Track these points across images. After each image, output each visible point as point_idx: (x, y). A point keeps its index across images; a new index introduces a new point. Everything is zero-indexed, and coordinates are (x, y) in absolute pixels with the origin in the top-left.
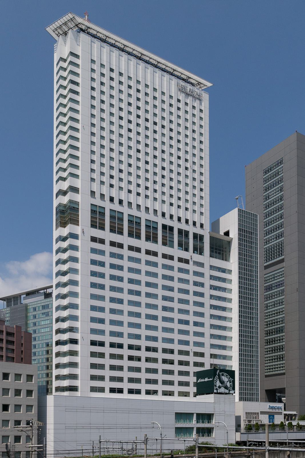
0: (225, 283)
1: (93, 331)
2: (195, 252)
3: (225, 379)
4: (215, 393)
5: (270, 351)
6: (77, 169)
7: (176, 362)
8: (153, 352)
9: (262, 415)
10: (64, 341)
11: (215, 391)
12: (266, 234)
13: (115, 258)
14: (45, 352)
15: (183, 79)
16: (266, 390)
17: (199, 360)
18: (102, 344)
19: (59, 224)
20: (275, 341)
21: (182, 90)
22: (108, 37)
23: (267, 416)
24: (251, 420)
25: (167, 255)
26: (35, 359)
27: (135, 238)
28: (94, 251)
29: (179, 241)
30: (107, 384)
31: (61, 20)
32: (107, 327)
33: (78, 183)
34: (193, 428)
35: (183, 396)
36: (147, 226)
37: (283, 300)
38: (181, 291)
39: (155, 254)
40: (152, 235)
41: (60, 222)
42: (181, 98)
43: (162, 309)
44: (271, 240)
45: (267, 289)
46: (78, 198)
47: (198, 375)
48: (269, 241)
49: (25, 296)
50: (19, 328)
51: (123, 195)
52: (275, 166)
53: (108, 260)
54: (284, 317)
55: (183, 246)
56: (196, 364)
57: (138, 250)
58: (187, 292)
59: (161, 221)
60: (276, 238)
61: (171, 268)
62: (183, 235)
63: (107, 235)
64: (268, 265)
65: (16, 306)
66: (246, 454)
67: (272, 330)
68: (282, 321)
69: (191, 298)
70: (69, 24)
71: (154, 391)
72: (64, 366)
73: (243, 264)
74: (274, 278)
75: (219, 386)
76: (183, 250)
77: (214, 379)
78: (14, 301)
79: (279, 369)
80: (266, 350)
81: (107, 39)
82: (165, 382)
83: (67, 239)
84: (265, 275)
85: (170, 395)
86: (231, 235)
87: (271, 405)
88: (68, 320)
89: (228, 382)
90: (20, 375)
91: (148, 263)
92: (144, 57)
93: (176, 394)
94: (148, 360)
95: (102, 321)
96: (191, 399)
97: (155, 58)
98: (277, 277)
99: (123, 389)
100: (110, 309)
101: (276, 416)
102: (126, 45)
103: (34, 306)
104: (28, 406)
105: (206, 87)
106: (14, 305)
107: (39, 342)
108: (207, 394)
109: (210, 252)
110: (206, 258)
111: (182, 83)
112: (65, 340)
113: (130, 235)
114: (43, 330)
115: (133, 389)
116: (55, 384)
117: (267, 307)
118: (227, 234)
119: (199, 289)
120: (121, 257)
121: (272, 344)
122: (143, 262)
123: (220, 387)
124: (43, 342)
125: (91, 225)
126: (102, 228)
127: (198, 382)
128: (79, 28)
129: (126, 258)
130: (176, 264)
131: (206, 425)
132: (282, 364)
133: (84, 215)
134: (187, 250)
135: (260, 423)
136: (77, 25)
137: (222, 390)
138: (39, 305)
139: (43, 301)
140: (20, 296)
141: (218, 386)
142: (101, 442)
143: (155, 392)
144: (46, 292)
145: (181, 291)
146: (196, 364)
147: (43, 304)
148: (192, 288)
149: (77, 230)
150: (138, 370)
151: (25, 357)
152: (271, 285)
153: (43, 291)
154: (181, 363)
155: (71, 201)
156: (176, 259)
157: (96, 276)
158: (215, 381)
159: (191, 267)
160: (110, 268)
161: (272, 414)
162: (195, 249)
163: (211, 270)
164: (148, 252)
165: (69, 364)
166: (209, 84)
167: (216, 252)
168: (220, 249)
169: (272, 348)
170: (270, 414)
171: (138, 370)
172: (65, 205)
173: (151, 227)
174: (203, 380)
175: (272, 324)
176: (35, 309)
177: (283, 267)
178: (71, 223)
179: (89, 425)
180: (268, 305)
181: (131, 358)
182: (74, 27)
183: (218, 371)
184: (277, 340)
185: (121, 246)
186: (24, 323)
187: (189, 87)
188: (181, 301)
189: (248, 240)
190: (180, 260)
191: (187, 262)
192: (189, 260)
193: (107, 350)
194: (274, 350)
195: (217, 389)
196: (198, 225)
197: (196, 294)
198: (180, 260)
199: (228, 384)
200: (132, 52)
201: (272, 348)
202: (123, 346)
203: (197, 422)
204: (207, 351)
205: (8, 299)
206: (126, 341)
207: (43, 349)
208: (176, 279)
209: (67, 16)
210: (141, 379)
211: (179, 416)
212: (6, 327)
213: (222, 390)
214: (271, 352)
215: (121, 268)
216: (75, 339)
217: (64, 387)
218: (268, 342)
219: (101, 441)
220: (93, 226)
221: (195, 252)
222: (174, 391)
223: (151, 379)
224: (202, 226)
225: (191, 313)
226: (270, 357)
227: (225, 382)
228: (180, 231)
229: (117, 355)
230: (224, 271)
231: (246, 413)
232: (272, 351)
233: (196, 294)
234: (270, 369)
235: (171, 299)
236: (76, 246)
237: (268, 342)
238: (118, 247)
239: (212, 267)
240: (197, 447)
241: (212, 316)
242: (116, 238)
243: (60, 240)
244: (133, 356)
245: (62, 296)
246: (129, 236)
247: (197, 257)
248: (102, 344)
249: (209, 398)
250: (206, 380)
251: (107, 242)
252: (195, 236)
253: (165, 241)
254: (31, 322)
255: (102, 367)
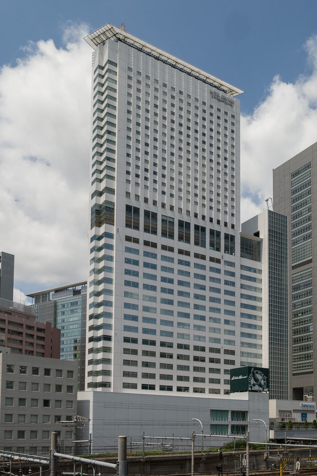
0: (256, 282)
1: (127, 328)
2: (226, 252)
3: (259, 377)
4: (249, 391)
5: (297, 350)
6: (113, 171)
7: (207, 360)
8: (184, 349)
9: (296, 414)
10: (98, 337)
11: (250, 389)
12: (294, 235)
13: (149, 257)
14: (73, 348)
15: (215, 87)
16: (293, 388)
17: (229, 357)
18: (135, 341)
19: (95, 223)
20: (302, 340)
21: (214, 96)
22: (144, 46)
23: (300, 414)
24: (284, 419)
25: (199, 254)
26: (63, 355)
27: (169, 238)
28: (128, 250)
29: (225, 245)
30: (140, 381)
31: (100, 30)
32: (140, 325)
33: (114, 185)
34: (228, 425)
35: (214, 393)
36: (163, 220)
37: (311, 300)
38: (212, 289)
39: (188, 253)
40: (184, 235)
41: (96, 221)
42: (213, 105)
43: (194, 307)
44: (299, 241)
45: (294, 289)
46: (114, 199)
47: (233, 372)
48: (297, 242)
49: (53, 292)
50: (48, 324)
51: (158, 197)
52: (303, 169)
53: (142, 259)
54: (312, 316)
55: (215, 246)
56: (227, 362)
57: (171, 249)
58: (218, 291)
59: (177, 217)
60: (304, 239)
61: (203, 267)
62: (214, 236)
63: (141, 235)
64: (296, 265)
65: (44, 303)
66: (284, 452)
67: (300, 329)
68: (310, 320)
69: (222, 297)
70: (107, 33)
71: (185, 387)
72: (97, 362)
73: (280, 266)
74: (302, 278)
75: (254, 384)
76: (214, 250)
77: (248, 377)
78: (43, 297)
79: (302, 368)
80: (294, 349)
81: (177, 65)
82: (196, 380)
83: (103, 238)
84: (292, 275)
85: (201, 392)
86: (261, 236)
87: (304, 404)
88: (102, 317)
89: (263, 380)
90: (61, 371)
91: (180, 262)
92: (179, 66)
93: (207, 391)
94: (179, 357)
95: (135, 318)
96: (222, 396)
97: (189, 66)
98: (304, 277)
99: (172, 386)
100: (143, 307)
101: (308, 415)
102: (161, 54)
103: (63, 303)
104: (21, 400)
105: (237, 94)
106: (43, 301)
107: (67, 338)
108: (241, 392)
109: (241, 252)
110: (236, 258)
111: (214, 89)
112: (99, 337)
113: (164, 234)
114: (71, 327)
115: (165, 386)
116: (88, 380)
117: (295, 306)
118: (257, 234)
119: (230, 288)
120: (154, 256)
121: (298, 343)
122: (176, 261)
123: (254, 385)
124: (71, 338)
125: (126, 224)
126: (137, 228)
127: (232, 379)
128: (117, 37)
129: (159, 257)
130: (207, 263)
131: (241, 423)
132: (310, 363)
133: (120, 215)
134: (218, 250)
135: (293, 421)
136: (115, 35)
137: (257, 388)
138: (68, 302)
139: (72, 298)
140: (49, 293)
141: (252, 383)
142: (144, 438)
143: (187, 389)
144: (75, 289)
145: (212, 289)
146: (227, 362)
147: (72, 301)
148: (223, 287)
149: (113, 230)
150: (170, 367)
151: (54, 352)
152: (299, 284)
153: (72, 288)
154: (212, 360)
155: (106, 202)
156: (208, 258)
157: (130, 275)
158: (250, 379)
159: (222, 266)
160: (144, 266)
161: (305, 412)
162: (226, 249)
163: (242, 269)
164: (181, 252)
165: (103, 361)
166: (241, 92)
167: (247, 253)
168: (251, 249)
169: (300, 347)
170: (303, 412)
171: (170, 367)
172: (100, 205)
173: (168, 222)
174: (237, 378)
175: (300, 323)
176: (63, 306)
177: (311, 268)
178: (106, 223)
179: (127, 421)
180: (296, 304)
181: (163, 355)
182: (112, 36)
183: (253, 369)
184: (305, 339)
185: (154, 245)
186: (53, 319)
187: (221, 93)
188: (212, 300)
189: (280, 242)
190: (212, 259)
191: (218, 261)
192: (220, 260)
193: (140, 347)
194: (302, 349)
195: (251, 387)
196: (229, 225)
197: (227, 292)
198: (212, 259)
199: (262, 382)
200: (142, 48)
201: (300, 347)
202: (137, 341)
203: (232, 420)
204: (237, 348)
205: (43, 294)
206: (158, 338)
207: (71, 345)
208: (207, 278)
209: (105, 27)
210: (155, 374)
211: (216, 413)
212: (37, 322)
213: (257, 388)
214: (299, 351)
215: (154, 267)
216: (108, 336)
217: (97, 383)
218: (296, 341)
219: (145, 437)
220: (128, 225)
221: (226, 252)
222: (205, 389)
223: (182, 376)
224: (233, 227)
225: (222, 311)
226: (297, 356)
227: (260, 380)
228: (212, 232)
229: (131, 350)
230: (255, 271)
231: (280, 411)
232: (300, 349)
233: (227, 292)
234: (298, 367)
235: (203, 298)
236: (111, 245)
237: (296, 341)
238: (151, 246)
239: (243, 267)
240: (248, 444)
241: (243, 315)
242: (150, 237)
243: (95, 239)
244: (165, 353)
245: (97, 293)
246: (162, 236)
247: (228, 257)
248: (135, 341)
249: (244, 396)
250: (241, 377)
251: (141, 242)
252: (227, 236)
253: (129, 224)
254: (60, 318)
255: (134, 363)
